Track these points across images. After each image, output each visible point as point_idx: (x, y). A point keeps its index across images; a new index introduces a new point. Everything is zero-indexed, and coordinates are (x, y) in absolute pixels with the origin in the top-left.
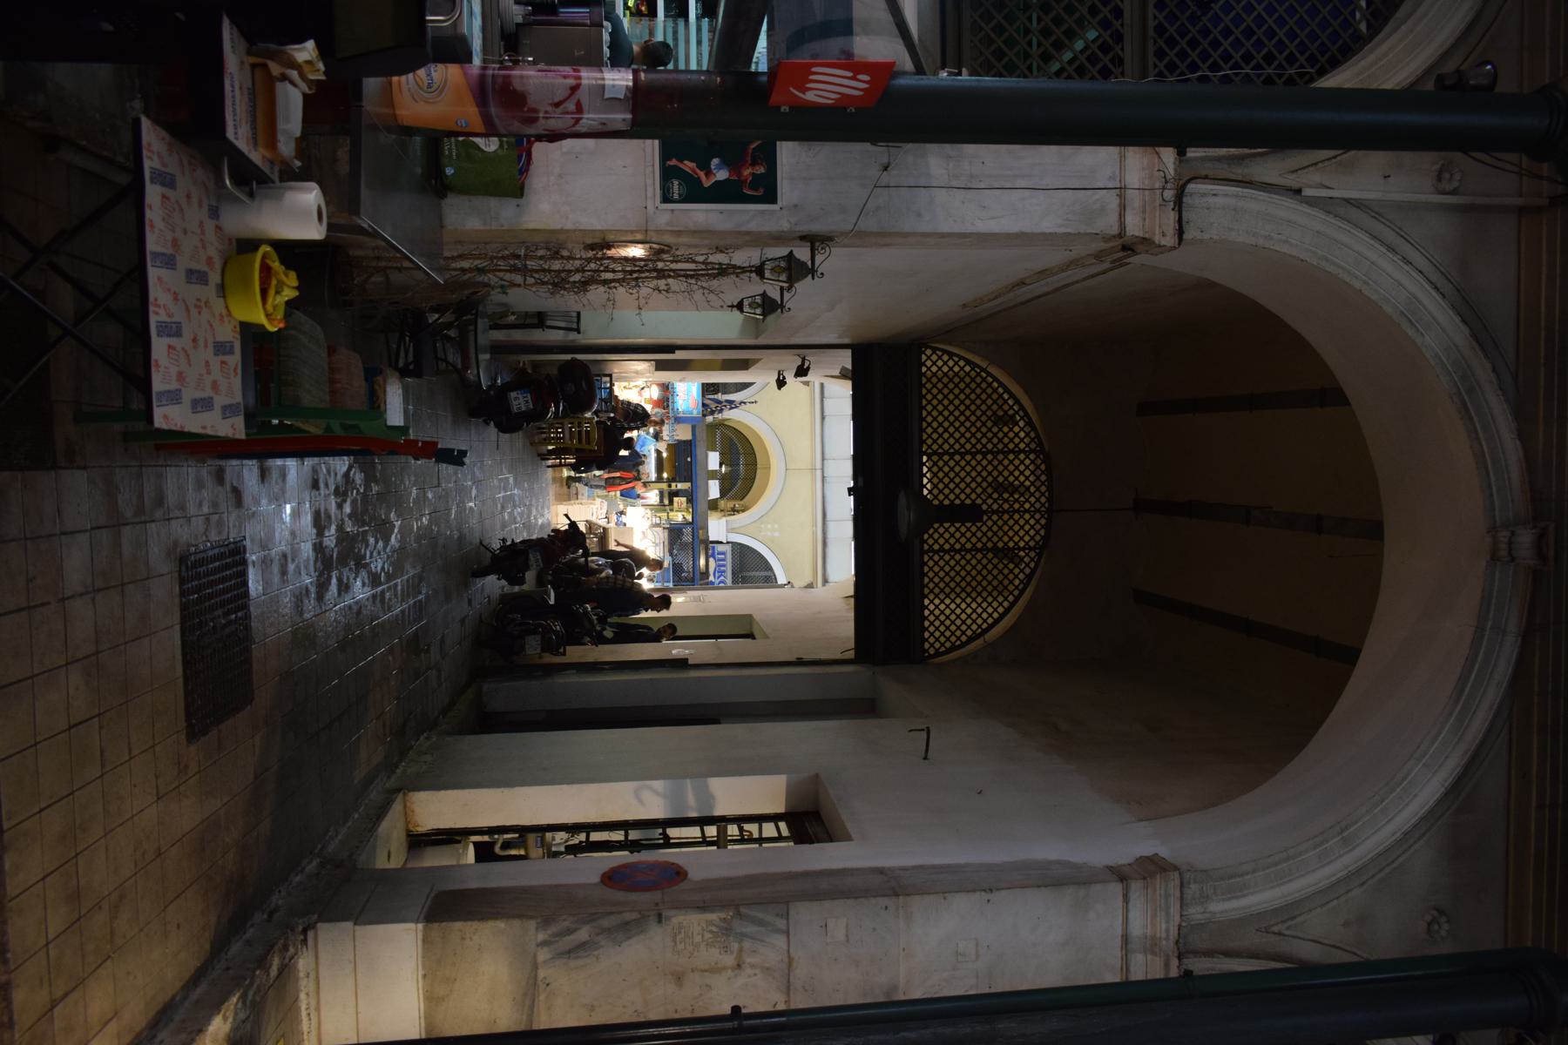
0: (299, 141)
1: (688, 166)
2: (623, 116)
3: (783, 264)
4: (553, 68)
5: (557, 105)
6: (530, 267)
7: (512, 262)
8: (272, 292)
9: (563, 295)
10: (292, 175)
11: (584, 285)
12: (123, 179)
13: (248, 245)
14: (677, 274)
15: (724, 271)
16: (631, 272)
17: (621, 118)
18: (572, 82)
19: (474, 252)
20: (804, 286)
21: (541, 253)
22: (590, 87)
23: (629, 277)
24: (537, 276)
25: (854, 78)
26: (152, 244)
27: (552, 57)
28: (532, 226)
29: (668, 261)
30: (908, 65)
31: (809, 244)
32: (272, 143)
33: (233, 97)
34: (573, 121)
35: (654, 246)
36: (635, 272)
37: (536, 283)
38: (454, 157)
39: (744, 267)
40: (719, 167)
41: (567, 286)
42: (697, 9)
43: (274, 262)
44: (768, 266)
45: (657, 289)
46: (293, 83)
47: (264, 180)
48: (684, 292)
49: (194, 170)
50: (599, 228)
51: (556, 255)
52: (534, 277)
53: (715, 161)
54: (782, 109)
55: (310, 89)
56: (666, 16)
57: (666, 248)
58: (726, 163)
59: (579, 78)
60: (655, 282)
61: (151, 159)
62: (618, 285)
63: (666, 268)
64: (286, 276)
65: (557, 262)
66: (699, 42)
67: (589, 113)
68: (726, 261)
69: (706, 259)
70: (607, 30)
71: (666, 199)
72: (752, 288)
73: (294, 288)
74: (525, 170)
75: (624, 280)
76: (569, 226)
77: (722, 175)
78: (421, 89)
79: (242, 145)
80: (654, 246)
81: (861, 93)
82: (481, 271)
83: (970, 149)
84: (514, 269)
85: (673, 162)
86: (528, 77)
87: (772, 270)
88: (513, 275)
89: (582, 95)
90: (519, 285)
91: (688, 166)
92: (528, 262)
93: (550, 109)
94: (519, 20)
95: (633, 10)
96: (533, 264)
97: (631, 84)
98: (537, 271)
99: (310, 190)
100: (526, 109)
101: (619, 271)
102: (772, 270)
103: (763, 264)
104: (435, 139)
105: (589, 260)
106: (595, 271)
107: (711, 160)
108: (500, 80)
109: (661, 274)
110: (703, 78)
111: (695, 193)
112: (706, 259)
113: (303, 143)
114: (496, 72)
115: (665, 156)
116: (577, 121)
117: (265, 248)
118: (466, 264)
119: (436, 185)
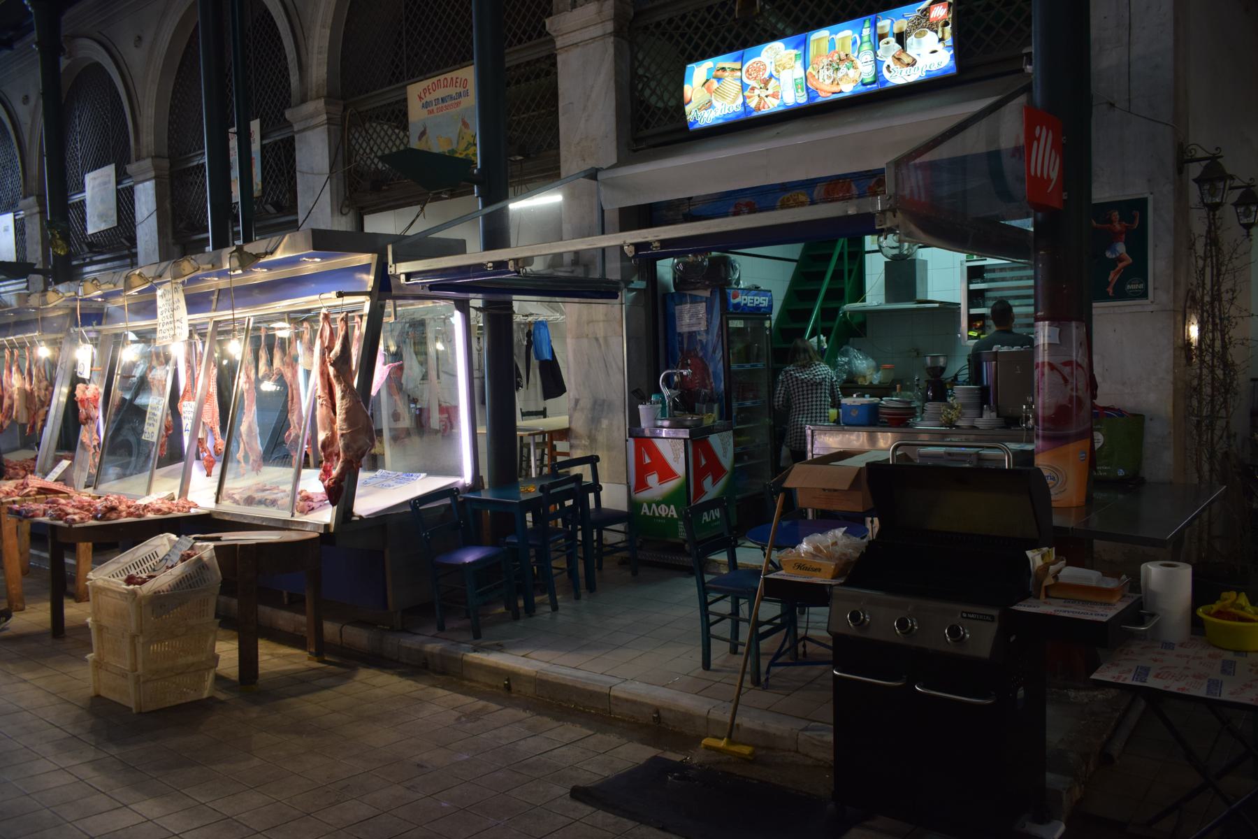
0: (1105, 574)
1: (1113, 277)
2: (1074, 331)
3: (1207, 187)
4: (1036, 384)
5: (1066, 381)
6: (1209, 413)
7: (1204, 428)
8: (1241, 613)
9: (1238, 384)
10: (1135, 584)
11: (1227, 366)
12: (1142, 705)
13: (1197, 625)
14: (1216, 283)
15: (1213, 241)
16: (1214, 324)
17: (1075, 330)
18: (1046, 370)
19: (1194, 460)
20: (1228, 165)
21: (1195, 403)
22: (1050, 355)
23: (1219, 327)
24: (1218, 407)
25: (1039, 140)
26: (1201, 692)
27: (1027, 387)
28: (1170, 409)
29: (1203, 292)
30: (1022, 99)
31: (1186, 165)
32: (1110, 592)
33: (1073, 612)
34: (1080, 369)
35: (1188, 304)
36: (1214, 321)
37: (1225, 407)
38: (1109, 468)
39: (1210, 223)
40: (1114, 251)
41: (1228, 381)
42: (978, 283)
43: (1212, 608)
44: (1208, 200)
45: (1232, 301)
46: (1059, 571)
47: (1139, 604)
48: (1235, 277)
49: (1132, 652)
50: (1172, 351)
51: (1197, 390)
52: (1219, 410)
53: (1108, 254)
54: (1066, 198)
55: (1063, 560)
56: (984, 307)
57: (1190, 294)
58: (1110, 245)
59: (1043, 363)
60: (1224, 303)
61: (1126, 678)
62: (1227, 336)
63: (1210, 293)
64: (1226, 599)
65: (1204, 390)
66: (1003, 279)
67: (1071, 356)
68: (1203, 239)
69: (1201, 257)
70: (999, 348)
71: (1144, 294)
72: (1228, 214)
73: (1238, 595)
74: (1120, 412)
75: (1222, 331)
76: (1171, 378)
77: (1121, 248)
78: (1055, 485)
79: (1111, 613)
80: (1188, 304)
81: (1050, 132)
82: (1212, 456)
83: (1094, 33)
84: (1211, 427)
85: (1110, 290)
86: (1044, 403)
87: (1213, 195)
88: (1217, 427)
89: (1057, 361)
90: (1228, 423)
91: (1113, 277)
92: (1204, 414)
93: (1069, 387)
94: (994, 415)
95: (980, 332)
96: (1205, 410)
97: (1047, 322)
98: (1213, 407)
99: (1148, 571)
100: (1070, 406)
101: (1213, 335)
102: (1213, 195)
103: (1206, 205)
104: (1095, 483)
105: (1202, 361)
106: (1213, 356)
107: (1108, 258)
108: (1047, 425)
109: (1216, 297)
110: (1040, 265)
111: (1139, 269)
112: (1201, 257)
113: (1110, 570)
114: (1040, 428)
115: (1105, 297)
116: (1079, 365)
117: (1200, 612)
118: (1206, 467)
119: (1134, 483)
